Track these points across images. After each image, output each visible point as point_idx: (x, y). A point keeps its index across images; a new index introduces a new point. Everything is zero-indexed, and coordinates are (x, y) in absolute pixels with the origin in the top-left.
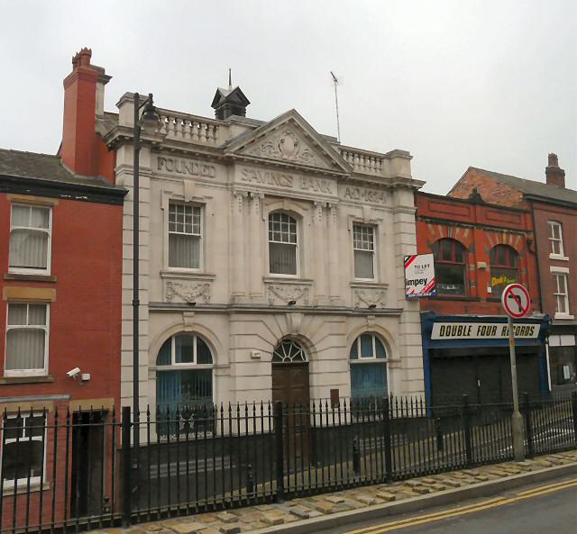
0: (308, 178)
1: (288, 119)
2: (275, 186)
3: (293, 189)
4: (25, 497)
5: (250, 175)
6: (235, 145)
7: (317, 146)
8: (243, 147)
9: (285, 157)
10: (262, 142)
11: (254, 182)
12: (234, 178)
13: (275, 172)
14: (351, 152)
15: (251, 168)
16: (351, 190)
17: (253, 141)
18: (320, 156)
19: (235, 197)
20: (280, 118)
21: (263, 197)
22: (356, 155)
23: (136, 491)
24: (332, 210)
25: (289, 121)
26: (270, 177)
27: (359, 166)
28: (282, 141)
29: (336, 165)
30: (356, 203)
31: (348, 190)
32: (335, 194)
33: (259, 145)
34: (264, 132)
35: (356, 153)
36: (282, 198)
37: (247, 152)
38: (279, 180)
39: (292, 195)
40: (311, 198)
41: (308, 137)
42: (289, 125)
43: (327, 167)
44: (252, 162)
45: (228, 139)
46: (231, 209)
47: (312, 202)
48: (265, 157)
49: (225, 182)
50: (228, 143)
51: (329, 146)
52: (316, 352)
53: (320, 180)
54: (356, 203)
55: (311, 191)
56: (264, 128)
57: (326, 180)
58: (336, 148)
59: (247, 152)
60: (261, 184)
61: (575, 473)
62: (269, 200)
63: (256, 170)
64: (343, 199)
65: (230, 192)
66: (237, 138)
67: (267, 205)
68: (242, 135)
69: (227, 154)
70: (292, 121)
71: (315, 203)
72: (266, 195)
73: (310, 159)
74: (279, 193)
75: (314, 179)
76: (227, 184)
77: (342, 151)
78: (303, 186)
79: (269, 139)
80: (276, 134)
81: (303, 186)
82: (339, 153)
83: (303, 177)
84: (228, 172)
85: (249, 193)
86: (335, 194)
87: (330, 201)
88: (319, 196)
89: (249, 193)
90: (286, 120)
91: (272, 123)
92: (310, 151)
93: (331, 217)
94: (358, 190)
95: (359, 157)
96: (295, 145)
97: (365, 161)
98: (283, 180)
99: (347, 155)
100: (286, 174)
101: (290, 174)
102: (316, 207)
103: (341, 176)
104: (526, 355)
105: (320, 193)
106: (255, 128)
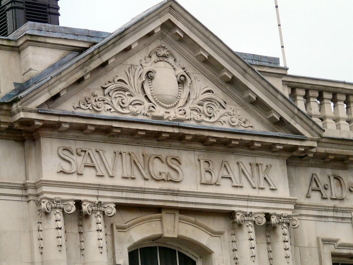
0: (216, 159)
1: (159, 22)
2: (140, 183)
3: (182, 187)
4: (156, 96)
5: (78, 161)
6: (38, 91)
7: (233, 82)
8: (57, 96)
9: (159, 111)
10: (102, 81)
11: (89, 177)
12: (40, 171)
13: (137, 151)
14: (314, 88)
15: (80, 145)
16: (323, 179)
17: (81, 80)
18: (242, 105)
19: (47, 214)
20: (140, 23)
21: (111, 210)
22: (326, 95)
23: (140, 135)
24: (280, 231)
25: (163, 26)
26: (126, 159)
27: (336, 120)
28: (150, 76)
29: (281, 123)
30: (335, 209)
31: (313, 179)
32: (283, 192)
33: (95, 88)
34: (104, 59)
35: (327, 90)
36: (158, 209)
37: (67, 107)
38: (147, 165)
39: (182, 202)
40: (236, 206)
41: (208, 62)
42: (162, 36)
43: (258, 128)
44: (82, 129)
45: (20, 80)
46: (36, 244)
47: (230, 215)
48: (109, 115)
49: (20, 181)
50: (21, 88)
51: (260, 77)
52: (157, 150)
53: (246, 161)
54: (335, 209)
55: (226, 188)
56: (100, 51)
57: (259, 160)
58: (277, 83)
59: (67, 107)
60: (106, 181)
61: (320, 264)
62: (128, 217)
63: (91, 147)
64: (306, 202)
65: (32, 204)
66: (42, 75)
67: (122, 229)
68: (53, 67)
69: (22, 115)
70: (168, 26)
71: (238, 218)
72: (120, 207)
73: (218, 112)
74: (151, 199)
75: (232, 160)
76: (24, 187)
77: (293, 90)
78: (207, 177)
79: (119, 73)
80: (135, 60)
81: (207, 177)
82: (286, 92)
83: (204, 156)
84: (26, 158)
85: (78, 204)
86: (283, 192)
87: (272, 208)
88: (248, 199)
89: (78, 204)
90: (155, 26)
91: (122, 35)
92: (219, 95)
93: (280, 246)
94: (337, 178)
95: (334, 100)
96: (181, 82)
97: (307, 103)
98: (158, 167)
99: (307, 97)
100: (164, 153)
101: (175, 153)
102: (240, 225)
103: (296, 148)
104: (325, 221)
105: (247, 191)
106: (81, 50)
